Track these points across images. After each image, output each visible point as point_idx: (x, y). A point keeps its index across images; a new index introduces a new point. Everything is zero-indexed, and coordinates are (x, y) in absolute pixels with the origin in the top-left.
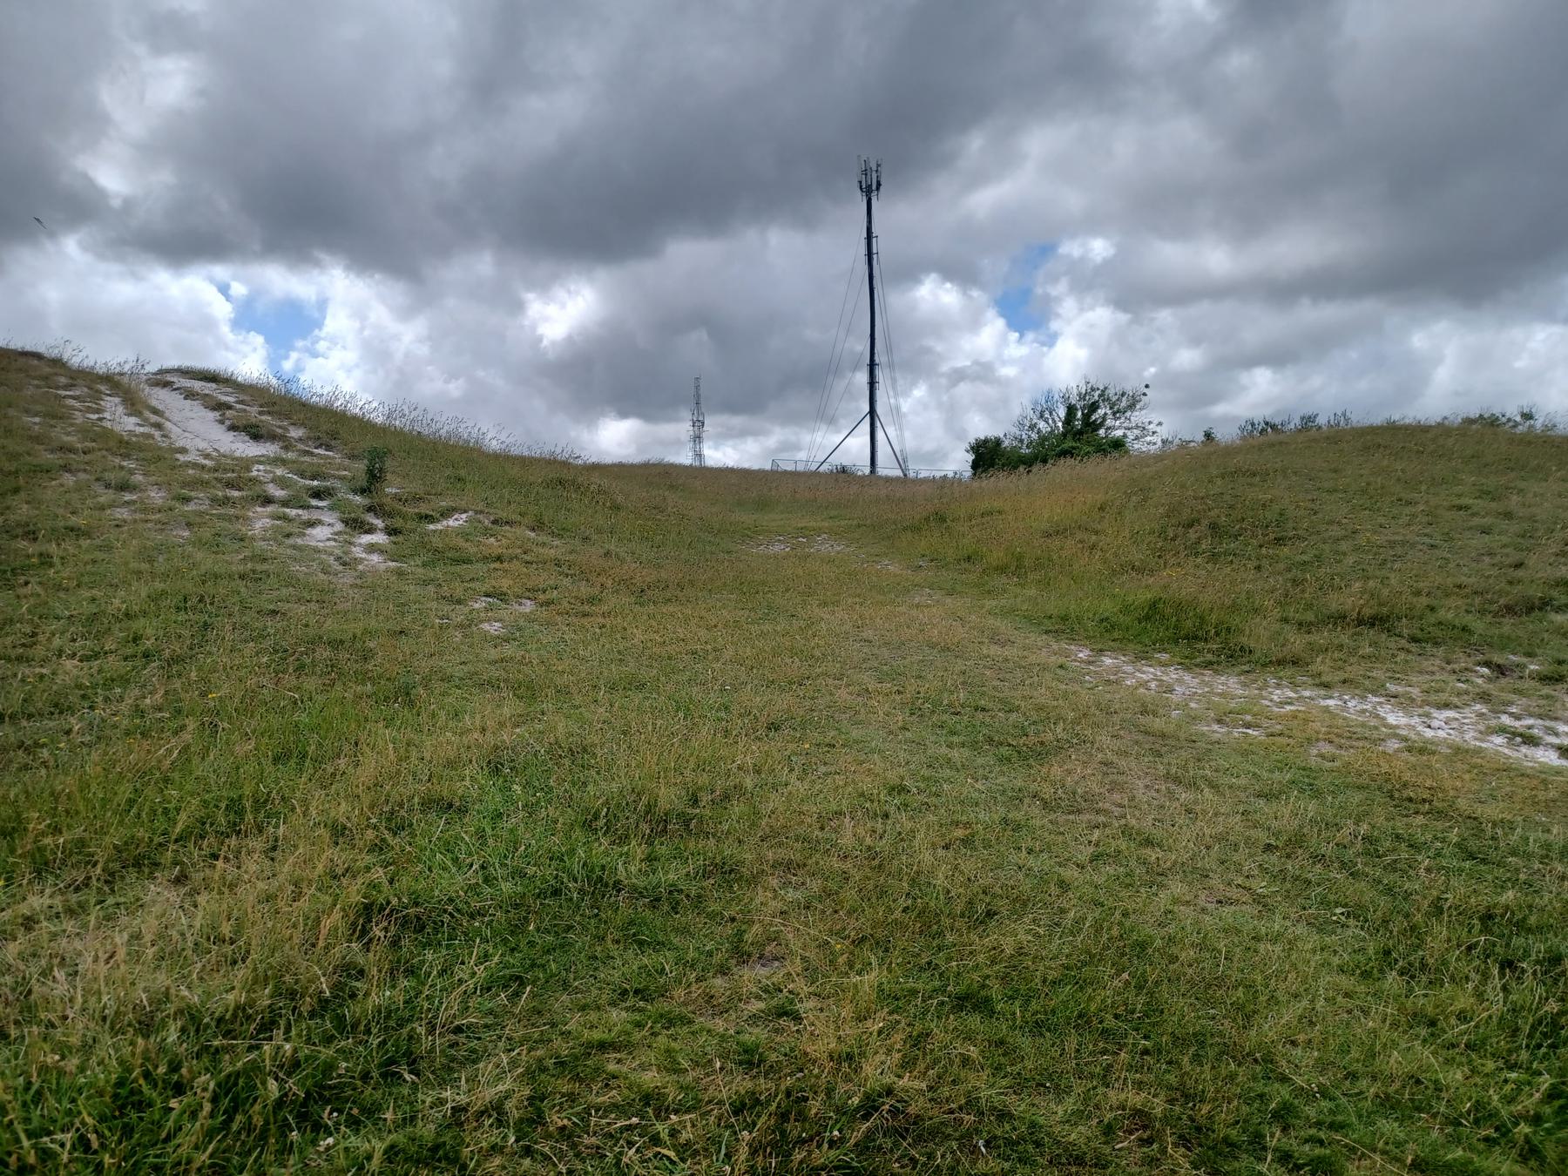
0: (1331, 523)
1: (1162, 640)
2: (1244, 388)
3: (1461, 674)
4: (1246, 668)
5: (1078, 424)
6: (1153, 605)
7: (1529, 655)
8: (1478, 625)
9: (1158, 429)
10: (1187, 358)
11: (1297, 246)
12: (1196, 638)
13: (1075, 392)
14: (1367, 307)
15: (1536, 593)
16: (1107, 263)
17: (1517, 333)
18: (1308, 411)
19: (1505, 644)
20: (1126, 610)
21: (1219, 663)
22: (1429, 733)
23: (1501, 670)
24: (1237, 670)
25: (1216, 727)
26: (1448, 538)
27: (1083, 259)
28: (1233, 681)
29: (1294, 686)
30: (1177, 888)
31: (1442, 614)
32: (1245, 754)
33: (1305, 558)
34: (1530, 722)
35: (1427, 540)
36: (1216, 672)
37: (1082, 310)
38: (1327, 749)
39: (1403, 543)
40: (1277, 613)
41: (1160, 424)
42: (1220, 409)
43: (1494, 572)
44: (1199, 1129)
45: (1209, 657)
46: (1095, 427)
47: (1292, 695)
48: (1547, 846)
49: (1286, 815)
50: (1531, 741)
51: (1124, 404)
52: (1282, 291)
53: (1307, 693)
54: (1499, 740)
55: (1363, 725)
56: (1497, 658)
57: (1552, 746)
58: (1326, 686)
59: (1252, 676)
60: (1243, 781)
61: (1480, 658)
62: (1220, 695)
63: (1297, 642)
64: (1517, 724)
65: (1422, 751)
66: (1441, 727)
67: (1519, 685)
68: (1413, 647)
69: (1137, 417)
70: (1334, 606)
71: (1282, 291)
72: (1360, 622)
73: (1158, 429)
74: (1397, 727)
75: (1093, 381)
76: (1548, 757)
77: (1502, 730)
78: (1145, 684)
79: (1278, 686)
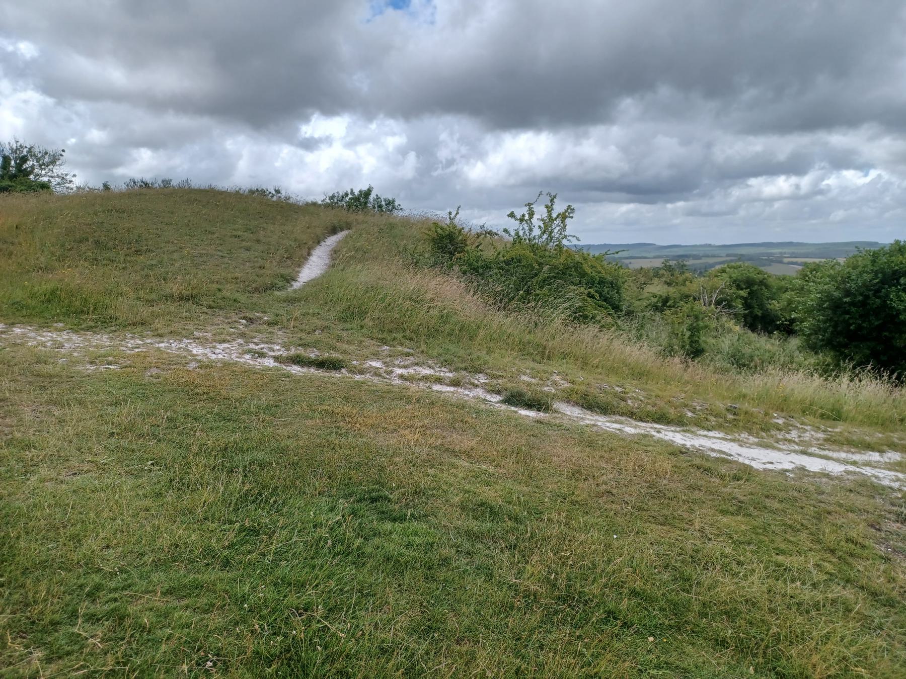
0: (168, 242)
1: (58, 314)
2: (135, 160)
3: (231, 324)
4: (113, 328)
5: (13, 170)
6: (53, 292)
7: (264, 312)
8: (242, 298)
9: (73, 179)
10: (96, 135)
11: (169, 77)
12: (82, 312)
13: (8, 147)
14: (205, 121)
15: (268, 281)
16: (34, 61)
17: (275, 148)
18: (167, 178)
19: (254, 307)
20: (33, 296)
21: (96, 327)
22: (214, 357)
23: (251, 321)
24: (108, 330)
25: (88, 367)
26: (230, 252)
27: (14, 54)
28: (105, 337)
29: (142, 337)
30: (44, 471)
31: (225, 293)
32: (104, 380)
33: (153, 262)
34: (262, 346)
35: (221, 254)
36: (95, 332)
37: (15, 90)
38: (154, 371)
39: (207, 255)
40: (133, 296)
41: (74, 176)
42: (120, 171)
43: (250, 270)
44: (33, 623)
45: (91, 324)
46: (27, 173)
47: (141, 342)
48: (259, 407)
49: (123, 414)
50: (262, 355)
51: (47, 160)
52: (157, 104)
53: (149, 341)
54: (247, 356)
55: (178, 356)
56: (250, 315)
57: (271, 356)
58: (161, 336)
59: (117, 334)
60: (102, 397)
61: (242, 315)
62: (94, 346)
63: (145, 312)
64: (257, 347)
65: (206, 367)
66: (221, 353)
67: (259, 327)
68: (209, 311)
69: (57, 170)
70: (168, 291)
71: (157, 104)
72: (181, 298)
73: (73, 179)
74: (197, 355)
75: (21, 142)
76: (269, 363)
77: (249, 351)
78: (43, 345)
79: (132, 338)
